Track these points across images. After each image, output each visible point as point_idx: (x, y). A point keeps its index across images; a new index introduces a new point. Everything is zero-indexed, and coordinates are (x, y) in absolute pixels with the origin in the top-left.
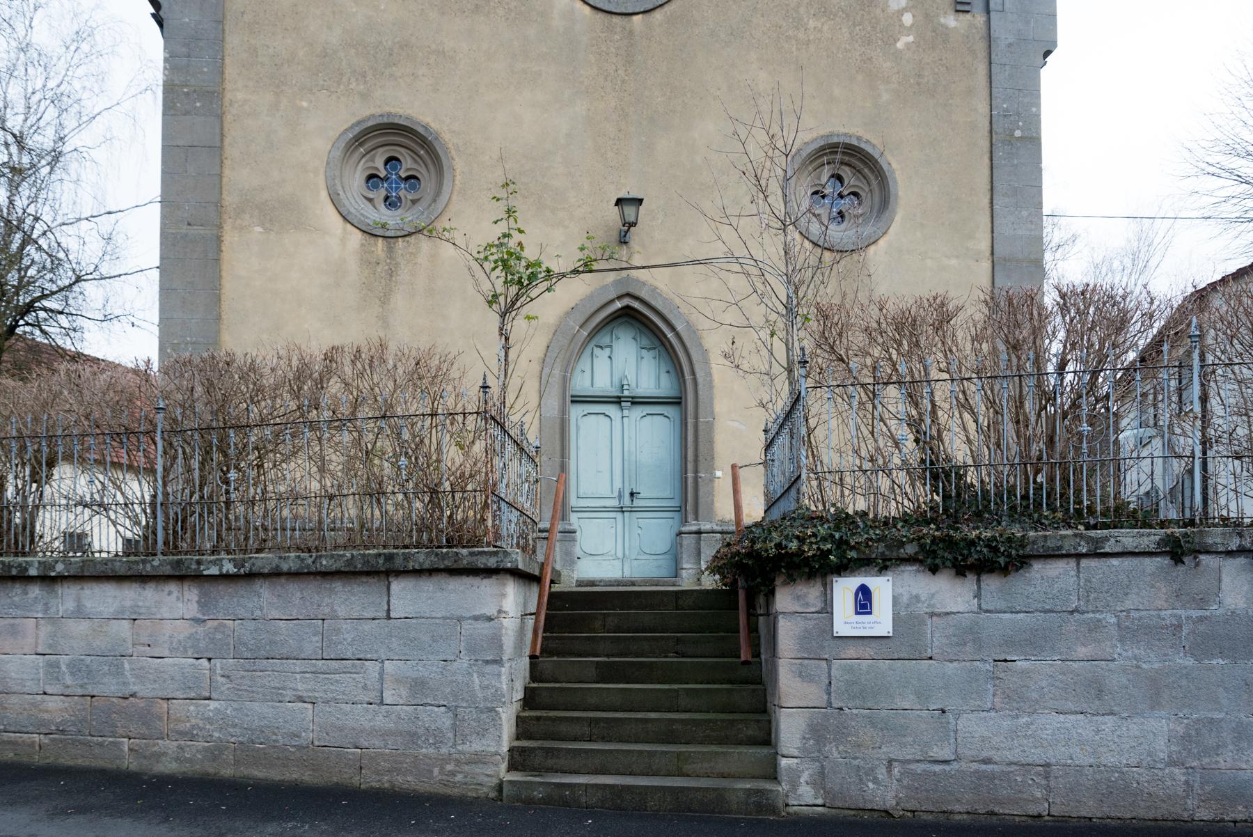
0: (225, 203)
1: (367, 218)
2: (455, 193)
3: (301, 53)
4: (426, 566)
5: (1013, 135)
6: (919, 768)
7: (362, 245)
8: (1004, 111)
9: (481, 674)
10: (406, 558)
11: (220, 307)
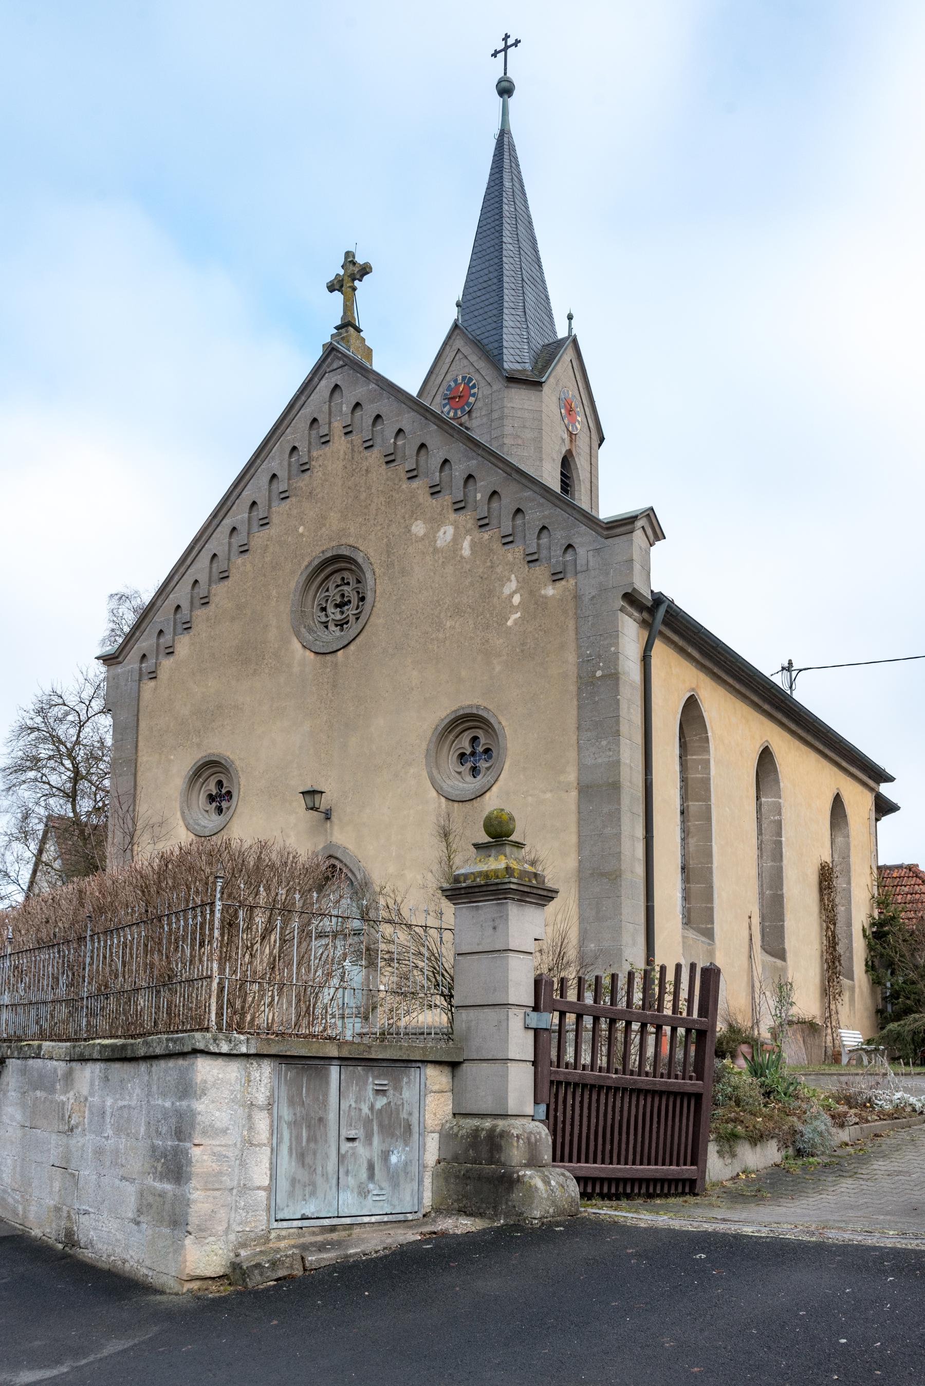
5: (595, 676)
8: (588, 657)
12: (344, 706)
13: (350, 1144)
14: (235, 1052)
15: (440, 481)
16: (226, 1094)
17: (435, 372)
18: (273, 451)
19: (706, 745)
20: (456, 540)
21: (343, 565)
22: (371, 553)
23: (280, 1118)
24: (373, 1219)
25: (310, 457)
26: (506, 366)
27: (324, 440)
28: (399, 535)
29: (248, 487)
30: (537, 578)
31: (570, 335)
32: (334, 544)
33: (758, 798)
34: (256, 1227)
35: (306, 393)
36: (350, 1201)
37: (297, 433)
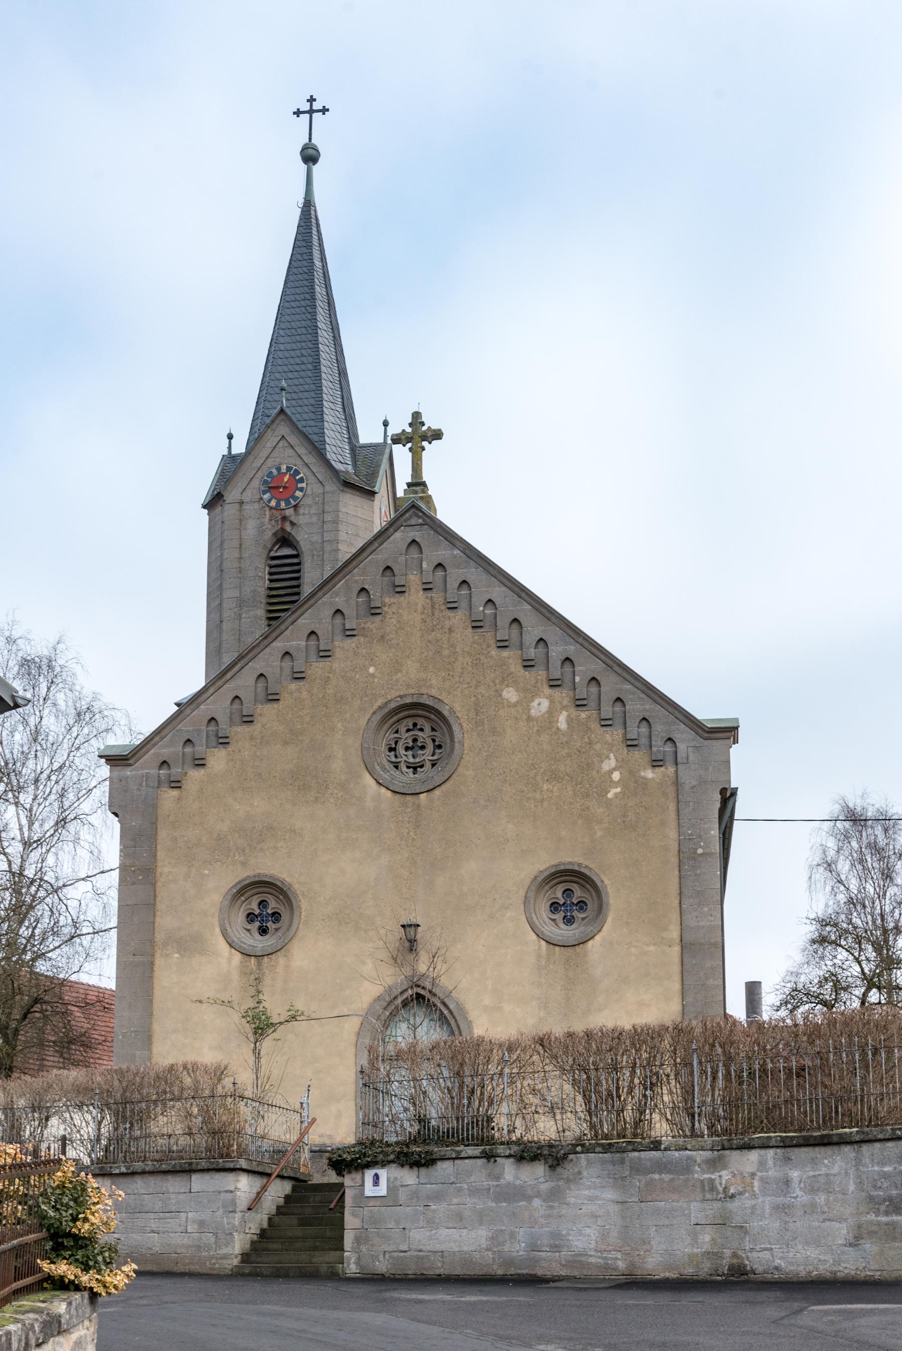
0: (157, 940)
1: (245, 944)
2: (301, 924)
3: (204, 839)
4: (205, 1168)
5: (696, 852)
6: (396, 1254)
7: (242, 962)
8: (689, 836)
9: (227, 1217)
10: (197, 1164)
11: (152, 1008)
12: (429, 846)
17: (253, 453)
18: (337, 587)
20: (552, 713)
21: (420, 712)
22: (457, 707)
28: (488, 697)
30: (636, 761)
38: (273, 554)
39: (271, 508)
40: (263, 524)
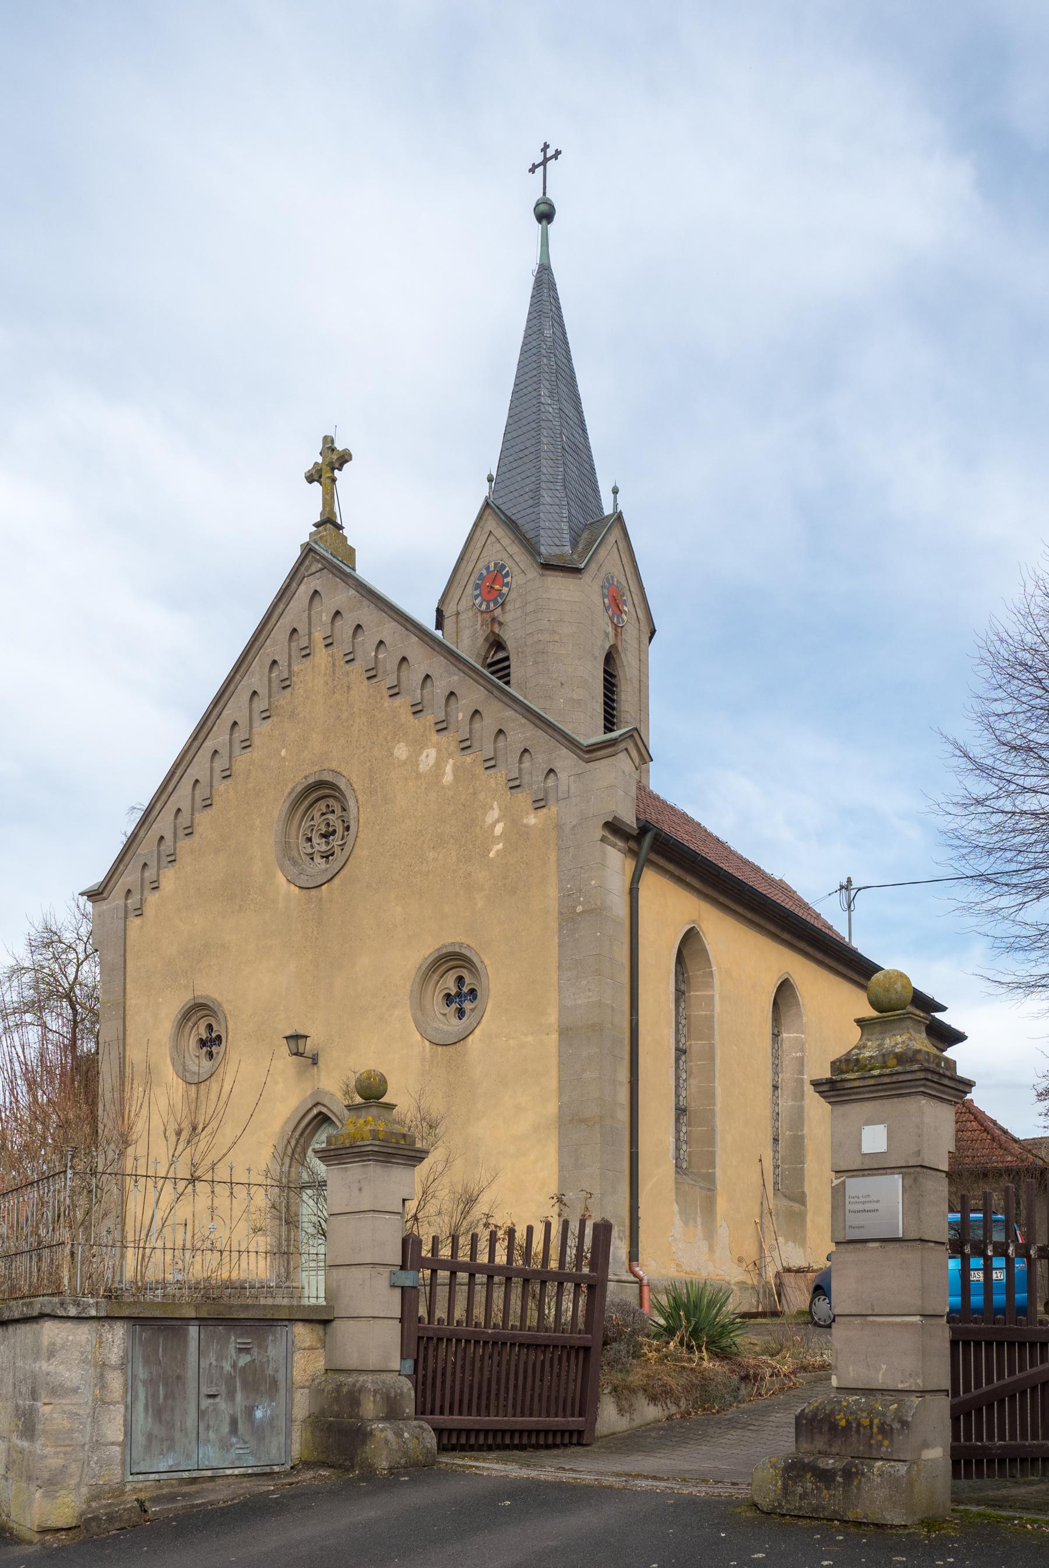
13: (211, 1401)
14: (83, 1315)
15: (422, 699)
16: (76, 1354)
19: (710, 980)
20: (439, 765)
21: (327, 792)
22: (354, 779)
23: (134, 1377)
24: (237, 1472)
25: (290, 672)
26: (543, 550)
27: (304, 653)
29: (228, 705)
31: (614, 513)
32: (317, 768)
33: (776, 1035)
34: (110, 1480)
35: (284, 600)
36: (211, 1454)
37: (276, 646)
38: (489, 661)
39: (482, 612)
40: (476, 630)
